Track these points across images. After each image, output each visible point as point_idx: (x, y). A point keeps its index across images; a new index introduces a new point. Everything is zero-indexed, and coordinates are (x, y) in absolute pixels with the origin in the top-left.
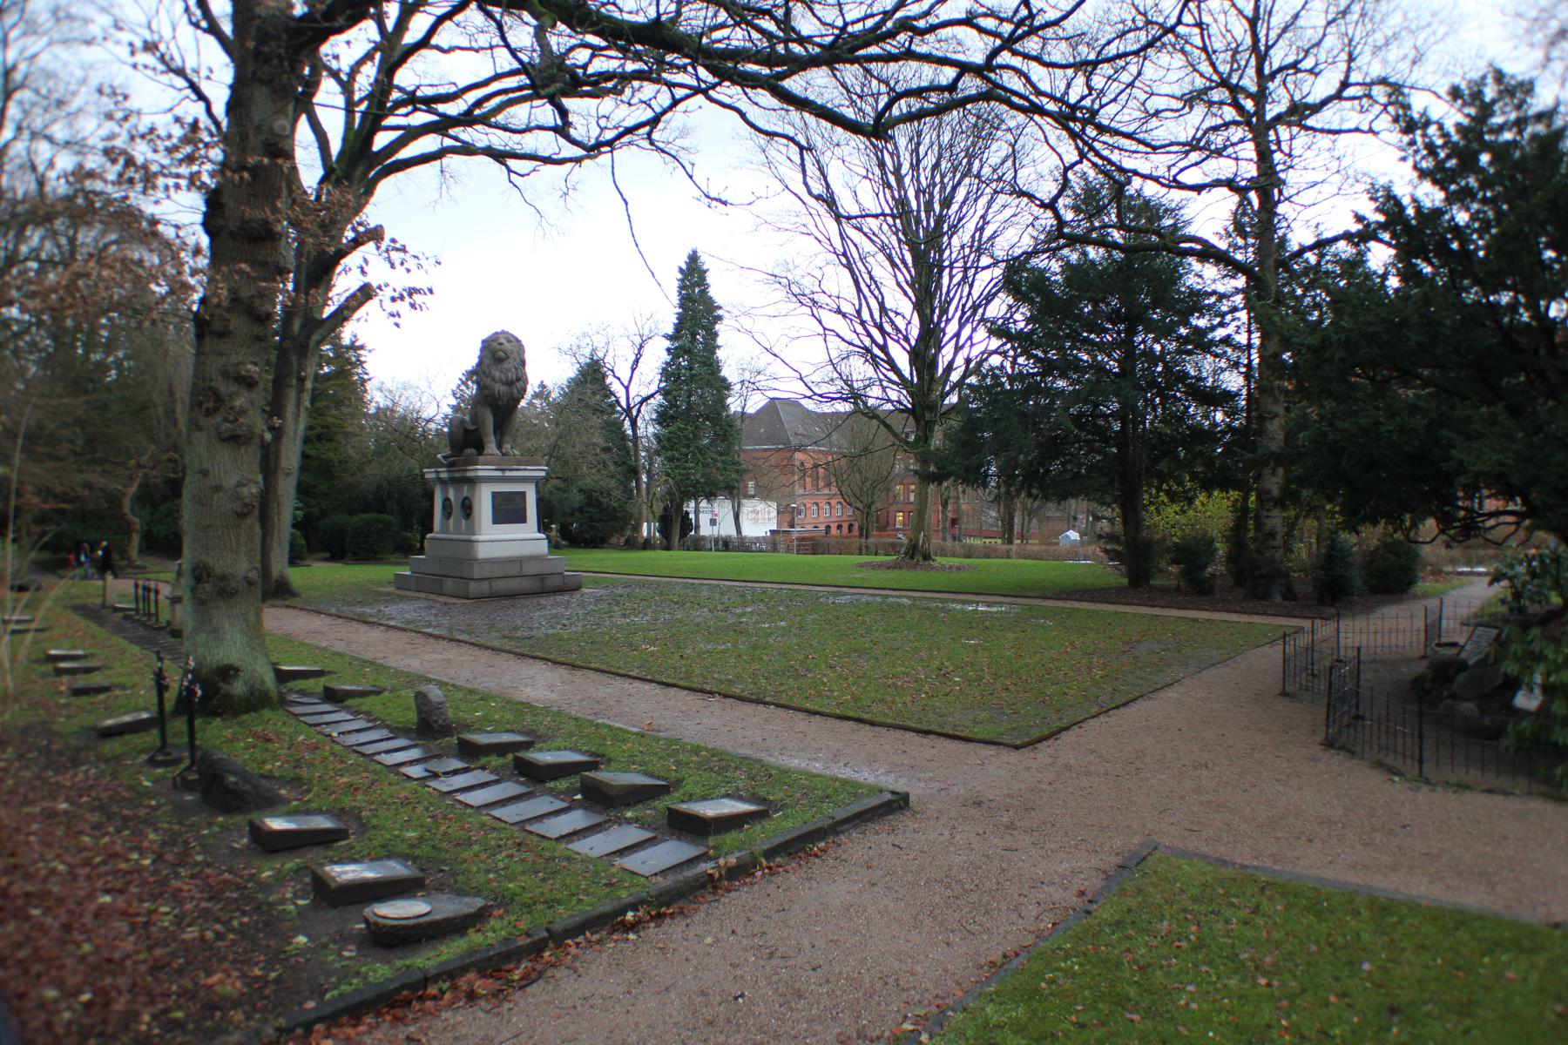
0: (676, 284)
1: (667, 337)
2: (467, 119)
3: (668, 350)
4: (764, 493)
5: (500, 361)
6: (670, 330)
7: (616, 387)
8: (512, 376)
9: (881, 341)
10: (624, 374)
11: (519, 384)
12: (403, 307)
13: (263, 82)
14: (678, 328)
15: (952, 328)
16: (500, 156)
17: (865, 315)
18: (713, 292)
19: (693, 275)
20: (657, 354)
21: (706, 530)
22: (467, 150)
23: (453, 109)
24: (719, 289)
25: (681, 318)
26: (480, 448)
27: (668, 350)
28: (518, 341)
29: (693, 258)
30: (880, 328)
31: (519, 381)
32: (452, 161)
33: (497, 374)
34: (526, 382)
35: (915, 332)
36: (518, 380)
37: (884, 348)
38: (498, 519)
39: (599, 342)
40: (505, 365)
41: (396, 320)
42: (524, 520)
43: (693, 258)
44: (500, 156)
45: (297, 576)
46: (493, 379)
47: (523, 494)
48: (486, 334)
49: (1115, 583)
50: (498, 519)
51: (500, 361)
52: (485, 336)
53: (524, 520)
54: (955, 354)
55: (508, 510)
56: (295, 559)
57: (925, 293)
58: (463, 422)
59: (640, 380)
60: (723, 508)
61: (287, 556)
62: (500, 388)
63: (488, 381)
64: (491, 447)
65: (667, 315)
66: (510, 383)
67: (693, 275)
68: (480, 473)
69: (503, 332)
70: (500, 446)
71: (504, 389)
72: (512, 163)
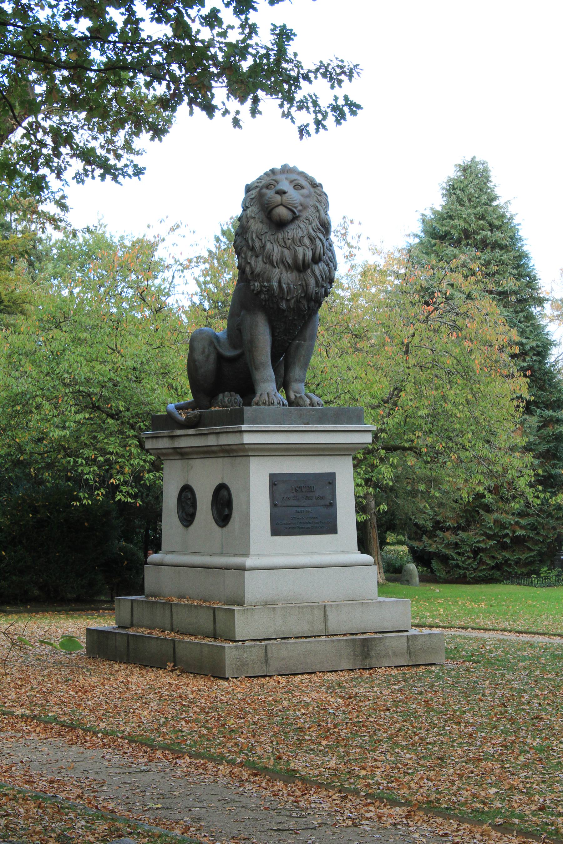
8: (304, 252)
42: (332, 529)
47: (329, 480)
51: (280, 225)
53: (332, 529)
55: (302, 508)
64: (267, 384)
66: (301, 267)
69: (286, 170)
71: (289, 278)
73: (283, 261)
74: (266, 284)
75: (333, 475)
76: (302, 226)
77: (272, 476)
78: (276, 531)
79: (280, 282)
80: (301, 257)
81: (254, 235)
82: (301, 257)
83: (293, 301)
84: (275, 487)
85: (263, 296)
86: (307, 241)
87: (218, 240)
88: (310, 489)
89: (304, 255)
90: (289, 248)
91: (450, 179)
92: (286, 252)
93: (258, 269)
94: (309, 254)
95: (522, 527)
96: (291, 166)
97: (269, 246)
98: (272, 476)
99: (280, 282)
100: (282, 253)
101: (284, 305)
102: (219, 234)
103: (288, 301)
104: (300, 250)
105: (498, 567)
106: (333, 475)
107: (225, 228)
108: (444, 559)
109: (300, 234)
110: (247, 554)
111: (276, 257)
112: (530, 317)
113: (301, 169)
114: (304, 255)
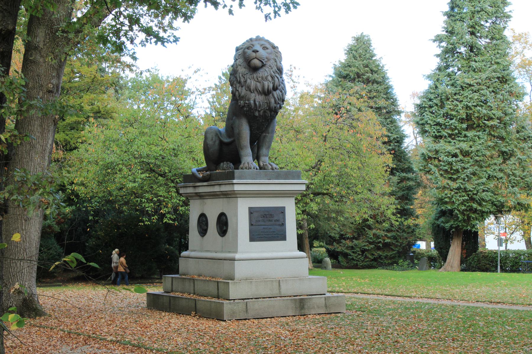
5: (255, 69)
8: (268, 85)
11: (276, 93)
21: (490, 243)
26: (237, 161)
28: (274, 47)
31: (274, 93)
33: (253, 84)
34: (283, 91)
36: (275, 89)
38: (256, 236)
40: (262, 73)
41: (272, 15)
42: (282, 237)
45: (48, 296)
46: (249, 89)
47: (282, 211)
48: (240, 41)
49: (443, 35)
50: (256, 236)
51: (255, 69)
52: (239, 43)
53: (282, 237)
55: (267, 226)
56: (45, 277)
58: (218, 133)
59: (411, 74)
61: (34, 275)
62: (257, 99)
63: (243, 91)
64: (247, 157)
66: (266, 93)
68: (237, 188)
69: (258, 39)
70: (257, 157)
71: (260, 99)
73: (256, 89)
74: (247, 102)
75: (284, 208)
76: (267, 70)
77: (250, 209)
78: (252, 239)
79: (255, 101)
80: (266, 87)
81: (241, 75)
82: (266, 87)
83: (262, 111)
84: (252, 215)
85: (245, 109)
86: (270, 78)
87: (220, 78)
88: (271, 216)
89: (268, 86)
90: (260, 82)
91: (349, 45)
92: (258, 84)
93: (243, 94)
94: (271, 86)
95: (388, 238)
96: (261, 37)
97: (249, 81)
98: (250, 209)
99: (255, 101)
100: (256, 85)
101: (257, 114)
102: (221, 75)
103: (259, 111)
104: (266, 83)
105: (375, 260)
106: (284, 208)
107: (224, 72)
108: (346, 255)
109: (266, 75)
110: (236, 252)
111: (252, 87)
112: (393, 122)
113: (266, 38)
114: (268, 86)
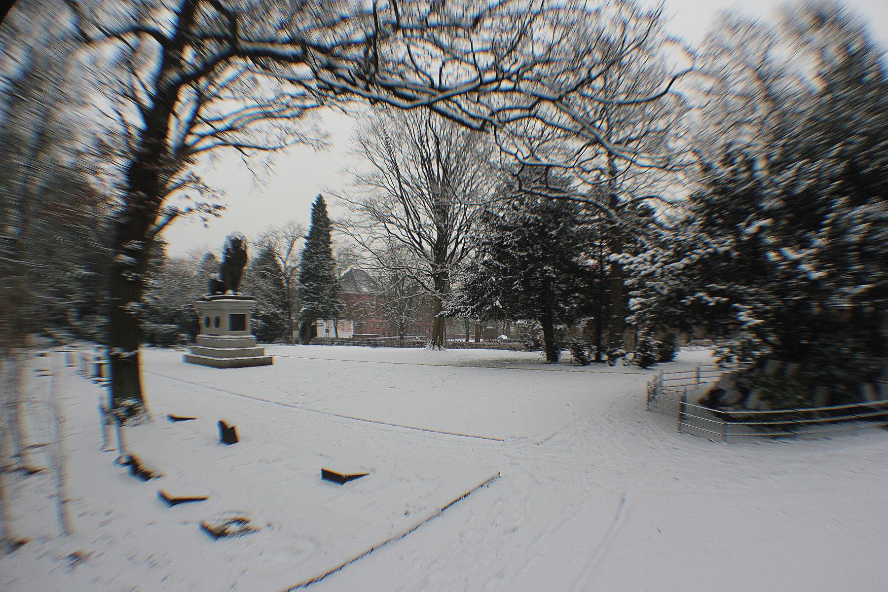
0: (311, 211)
1: (306, 238)
2: (231, 129)
3: (306, 244)
4: (349, 317)
6: (307, 234)
7: (280, 262)
9: (418, 240)
10: (284, 257)
12: (210, 216)
13: (224, 58)
14: (311, 233)
15: (454, 234)
16: (238, 146)
17: (411, 227)
18: (329, 216)
19: (319, 207)
20: (301, 245)
22: (226, 144)
23: (219, 126)
24: (333, 213)
25: (313, 228)
27: (306, 244)
29: (320, 200)
30: (419, 234)
32: (218, 151)
35: (435, 237)
37: (420, 244)
39: (272, 239)
43: (320, 200)
44: (238, 146)
53: (244, 328)
54: (456, 246)
57: (441, 212)
60: (331, 323)
65: (307, 223)
67: (319, 207)
72: (245, 150)
